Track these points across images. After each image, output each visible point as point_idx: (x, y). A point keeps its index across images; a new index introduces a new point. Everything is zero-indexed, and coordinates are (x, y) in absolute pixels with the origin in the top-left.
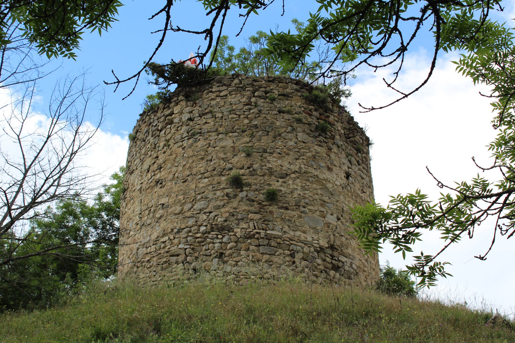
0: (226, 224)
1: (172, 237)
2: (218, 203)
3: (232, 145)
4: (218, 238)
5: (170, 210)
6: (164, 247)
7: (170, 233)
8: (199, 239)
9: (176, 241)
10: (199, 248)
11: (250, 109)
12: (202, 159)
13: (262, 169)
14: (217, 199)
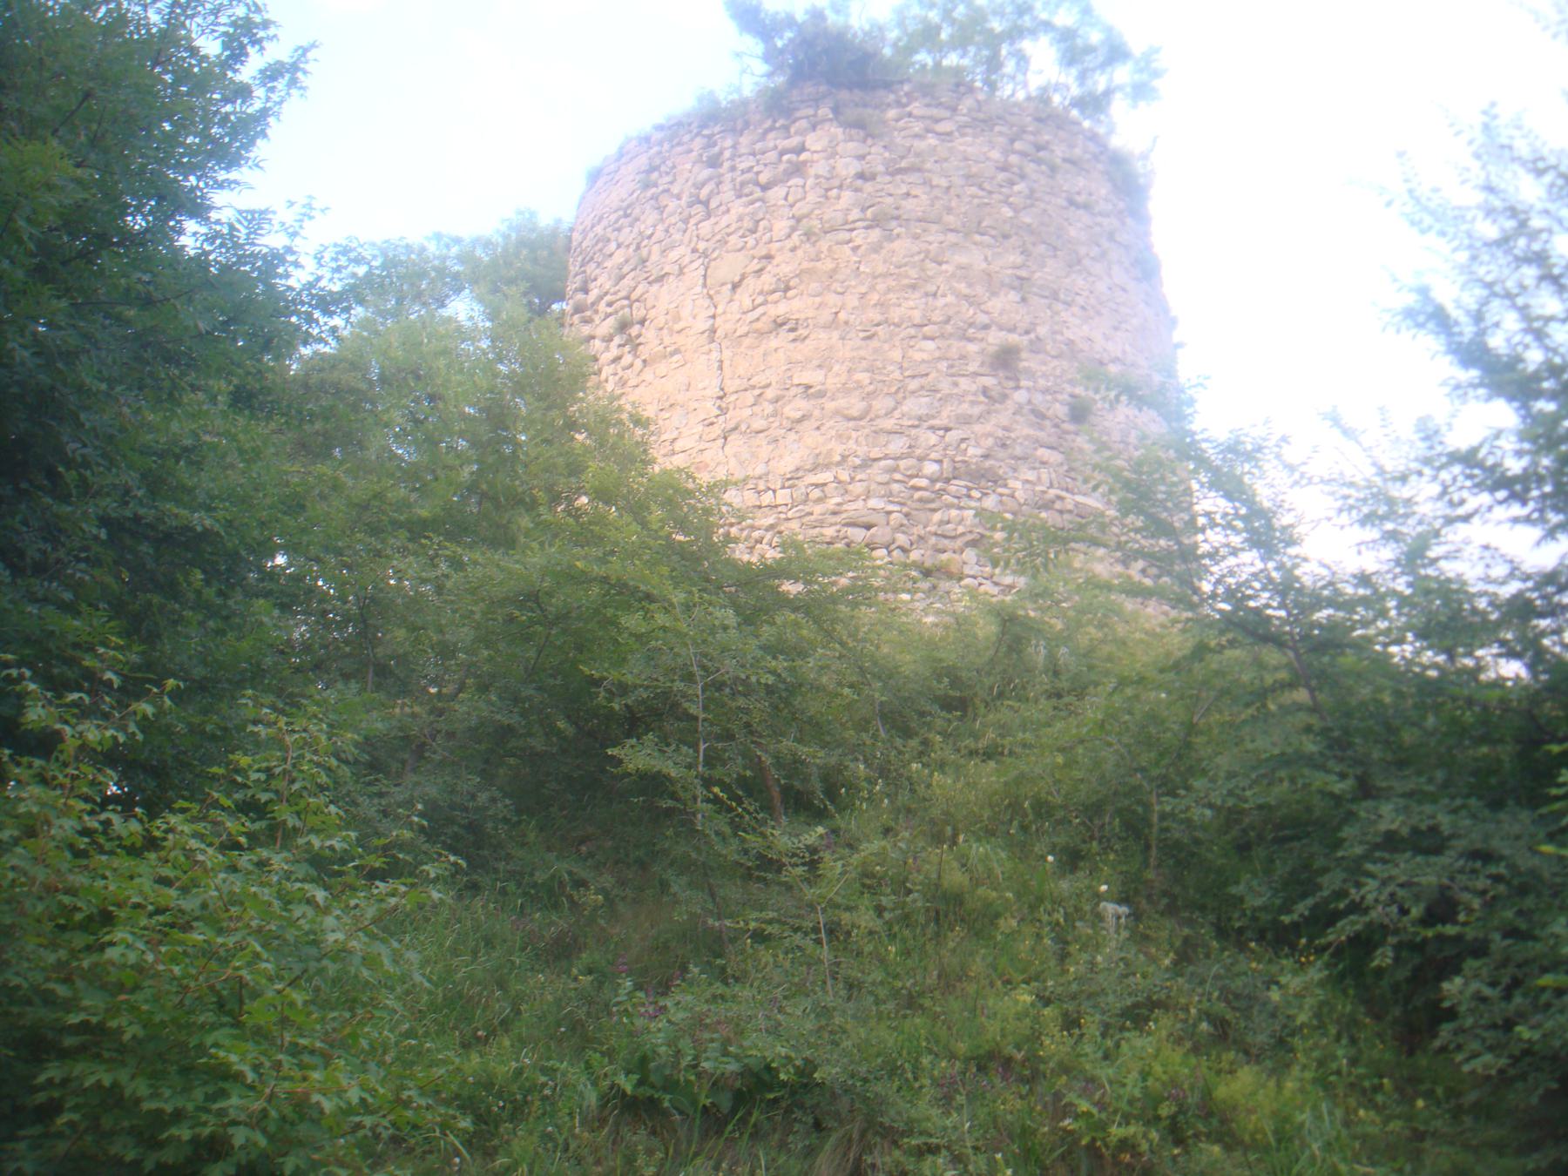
0: (988, 463)
1: (845, 476)
2: (965, 408)
3: (984, 265)
4: (969, 496)
5: (830, 406)
6: (820, 500)
7: (839, 464)
8: (925, 494)
9: (858, 488)
10: (922, 516)
11: (1012, 183)
12: (914, 287)
13: (1055, 341)
14: (961, 398)
